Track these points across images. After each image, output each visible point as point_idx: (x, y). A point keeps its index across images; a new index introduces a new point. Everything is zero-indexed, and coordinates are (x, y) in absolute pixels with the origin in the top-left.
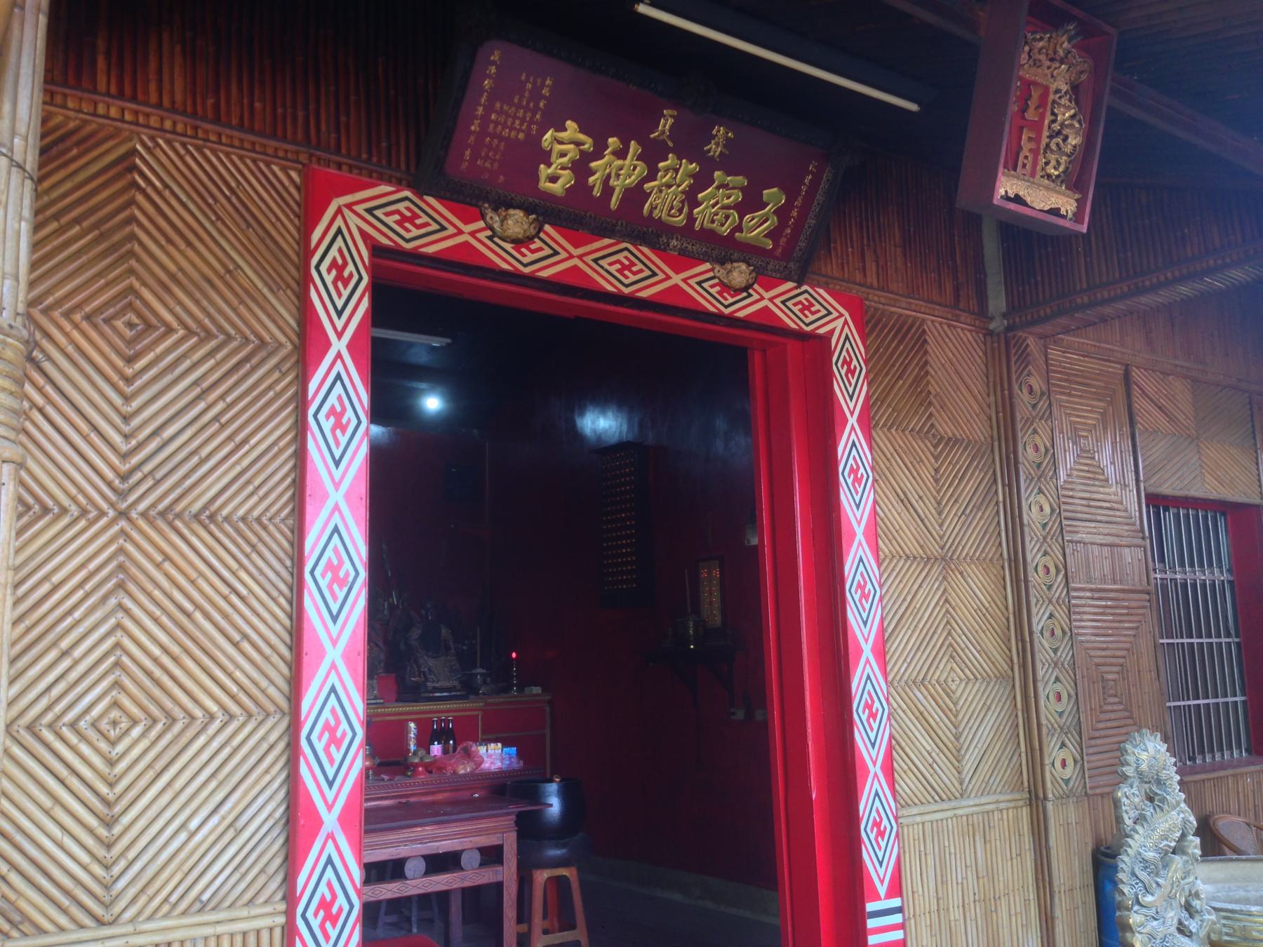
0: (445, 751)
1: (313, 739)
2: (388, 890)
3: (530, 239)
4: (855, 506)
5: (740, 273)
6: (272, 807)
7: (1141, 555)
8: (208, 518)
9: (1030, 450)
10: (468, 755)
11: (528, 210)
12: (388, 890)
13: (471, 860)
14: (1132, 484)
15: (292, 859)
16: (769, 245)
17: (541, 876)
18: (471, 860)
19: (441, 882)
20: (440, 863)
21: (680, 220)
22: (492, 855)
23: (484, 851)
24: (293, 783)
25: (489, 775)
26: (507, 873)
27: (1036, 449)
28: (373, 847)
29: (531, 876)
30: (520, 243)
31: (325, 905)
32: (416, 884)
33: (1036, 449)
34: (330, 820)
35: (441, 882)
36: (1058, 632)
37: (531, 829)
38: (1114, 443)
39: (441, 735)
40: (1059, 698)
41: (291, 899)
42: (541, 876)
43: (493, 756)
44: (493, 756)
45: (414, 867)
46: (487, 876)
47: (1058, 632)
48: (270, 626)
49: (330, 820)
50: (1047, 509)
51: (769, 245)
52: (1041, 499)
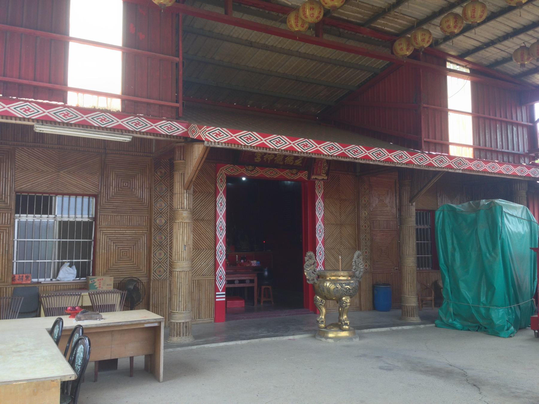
0: (244, 262)
1: (218, 253)
2: (231, 286)
3: (253, 170)
4: (320, 214)
5: (294, 171)
6: (212, 263)
7: (396, 223)
8: (202, 220)
9: (363, 201)
10: (249, 262)
11: (252, 165)
12: (231, 286)
13: (248, 281)
14: (395, 207)
15: (216, 270)
16: (301, 165)
17: (263, 287)
18: (248, 281)
19: (242, 285)
20: (241, 281)
21: (281, 163)
22: (252, 281)
23: (250, 280)
24: (215, 259)
25: (254, 267)
26: (255, 285)
27: (365, 201)
28: (229, 277)
29: (122, 108)
30: (251, 171)
31: (220, 277)
32: (237, 285)
33: (365, 201)
34: (221, 265)
35: (242, 285)
36: (367, 239)
37: (260, 277)
38: (390, 198)
39: (243, 258)
40: (366, 252)
41: (216, 276)
42: (263, 287)
43: (254, 263)
44: (254, 263)
45: (236, 282)
46: (251, 285)
47: (367, 239)
48: (212, 236)
49: (221, 265)
50: (367, 214)
51: (301, 165)
52: (366, 212)
